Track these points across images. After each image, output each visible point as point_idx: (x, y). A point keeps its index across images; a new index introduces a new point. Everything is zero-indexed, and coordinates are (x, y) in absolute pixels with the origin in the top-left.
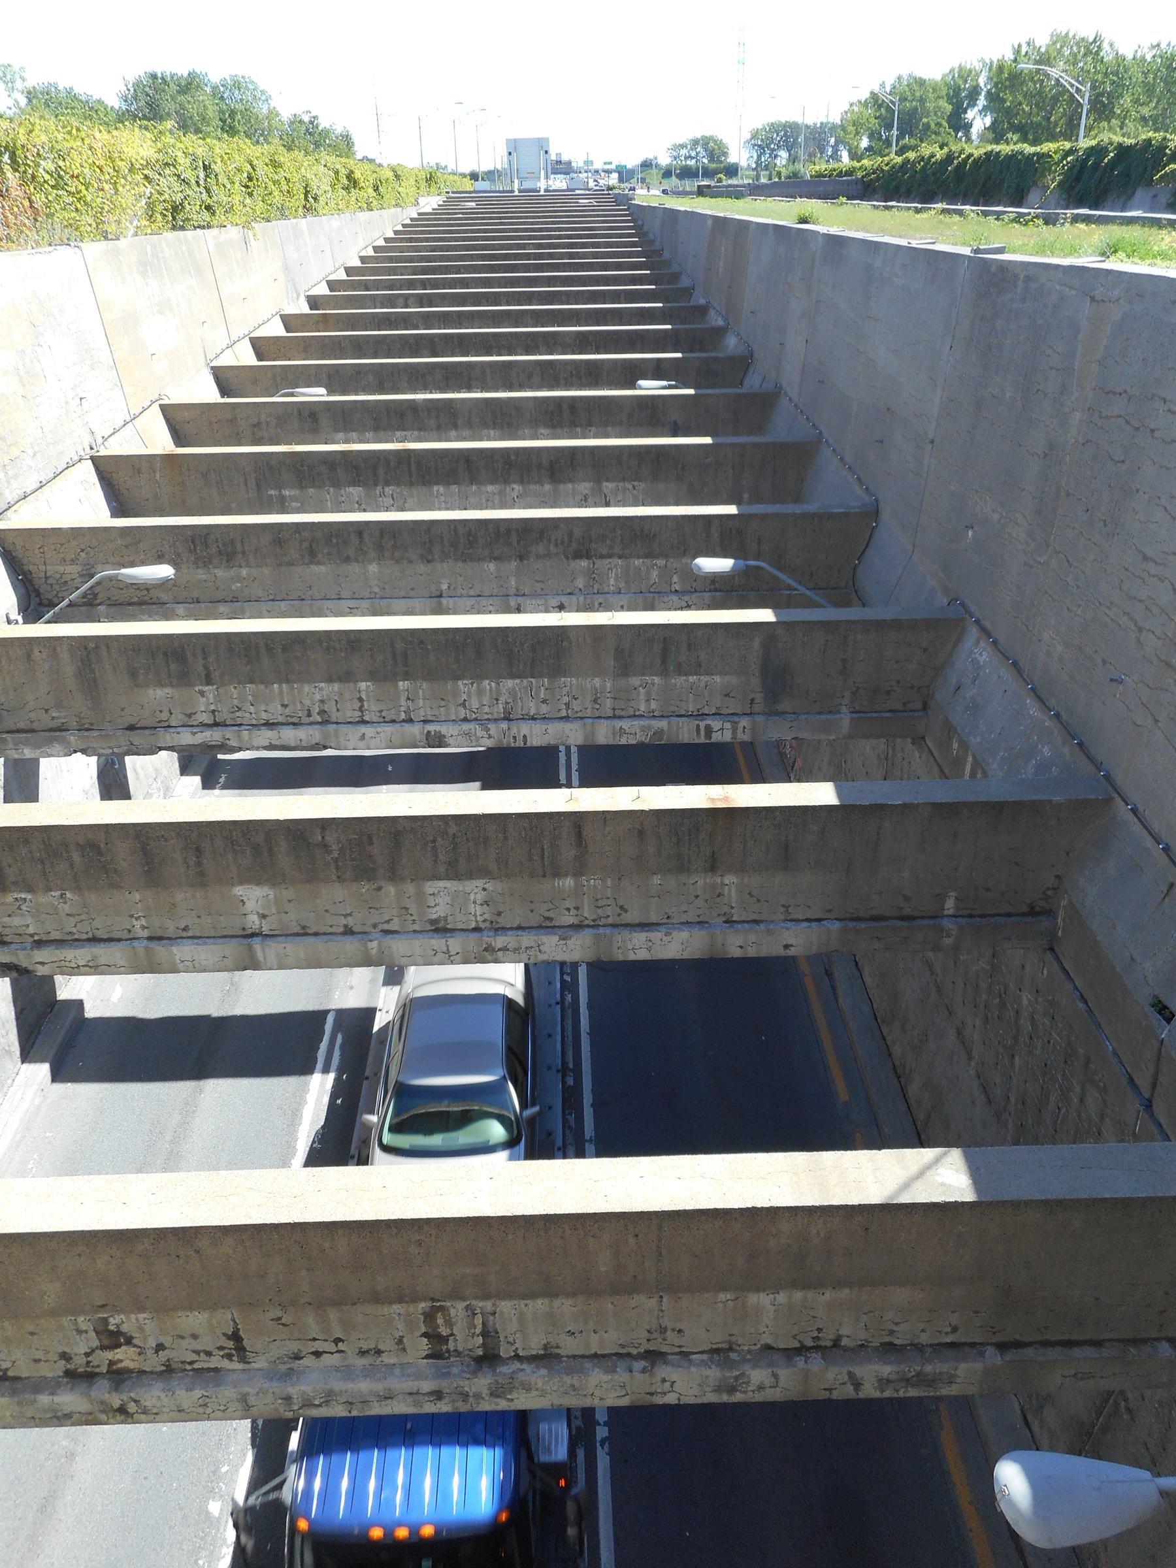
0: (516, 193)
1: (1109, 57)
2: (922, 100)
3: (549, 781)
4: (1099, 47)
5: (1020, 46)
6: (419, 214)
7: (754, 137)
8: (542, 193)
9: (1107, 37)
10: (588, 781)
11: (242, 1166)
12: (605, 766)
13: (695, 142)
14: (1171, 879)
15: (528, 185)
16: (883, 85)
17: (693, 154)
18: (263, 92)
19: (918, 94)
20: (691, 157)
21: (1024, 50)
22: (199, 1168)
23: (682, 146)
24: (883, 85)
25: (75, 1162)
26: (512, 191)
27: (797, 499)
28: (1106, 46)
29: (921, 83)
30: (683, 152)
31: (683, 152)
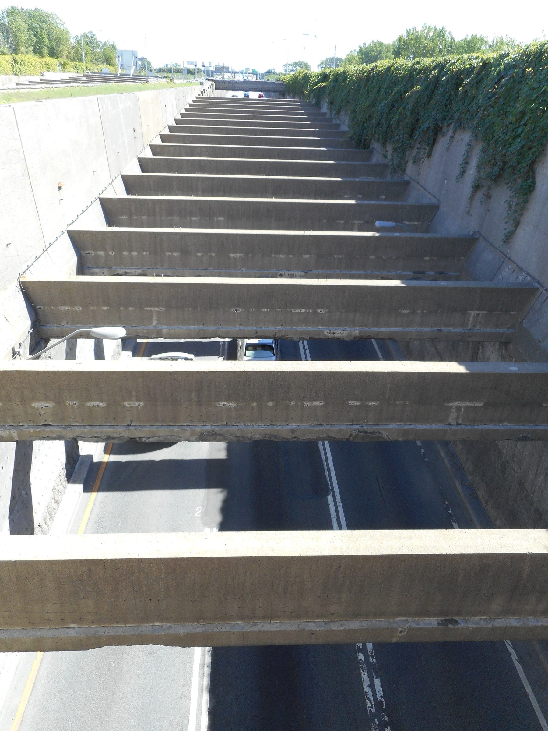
0: (119, 76)
1: (448, 39)
2: (380, 52)
3: (296, 357)
4: (444, 34)
5: (410, 30)
6: (41, 80)
7: (322, 64)
8: (131, 76)
9: (448, 29)
10: (316, 357)
11: (184, 529)
12: (322, 350)
13: (296, 64)
14: (2, 471)
15: (125, 72)
16: (365, 44)
17: (295, 69)
18: (61, 20)
19: (378, 49)
20: (293, 70)
21: (412, 32)
22: (158, 530)
23: (290, 65)
24: (365, 44)
25: (101, 526)
26: (129, 75)
27: (427, 231)
28: (447, 34)
29: (380, 44)
30: (290, 68)
31: (290, 68)
